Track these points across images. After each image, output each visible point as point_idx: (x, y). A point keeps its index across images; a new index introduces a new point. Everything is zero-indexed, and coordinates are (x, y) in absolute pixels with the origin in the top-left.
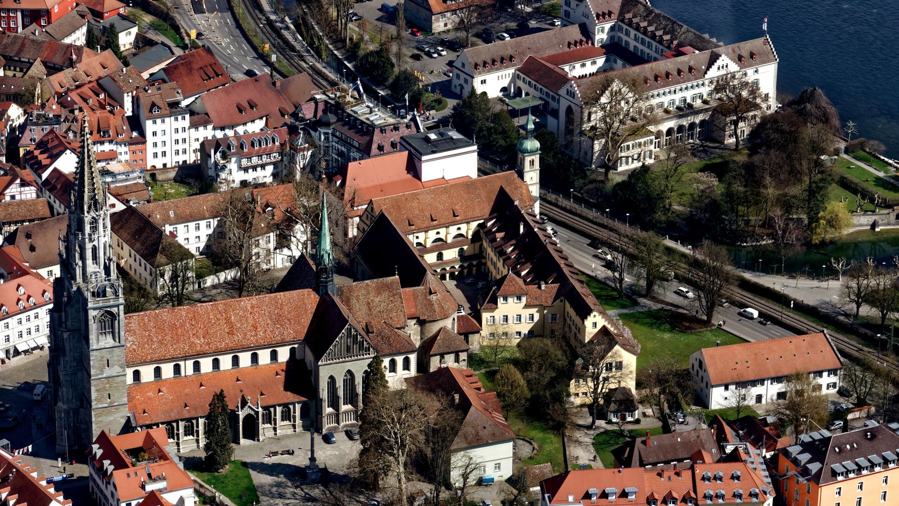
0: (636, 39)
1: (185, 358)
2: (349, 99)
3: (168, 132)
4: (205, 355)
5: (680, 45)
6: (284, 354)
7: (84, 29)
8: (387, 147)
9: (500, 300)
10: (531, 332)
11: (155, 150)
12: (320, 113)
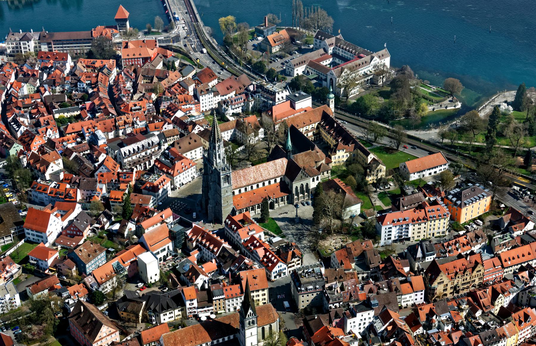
0: (342, 52)
1: (248, 186)
2: (264, 83)
4: (254, 184)
5: (359, 54)
6: (278, 180)
7: (162, 62)
8: (281, 99)
9: (337, 152)
10: (347, 160)
12: (255, 89)
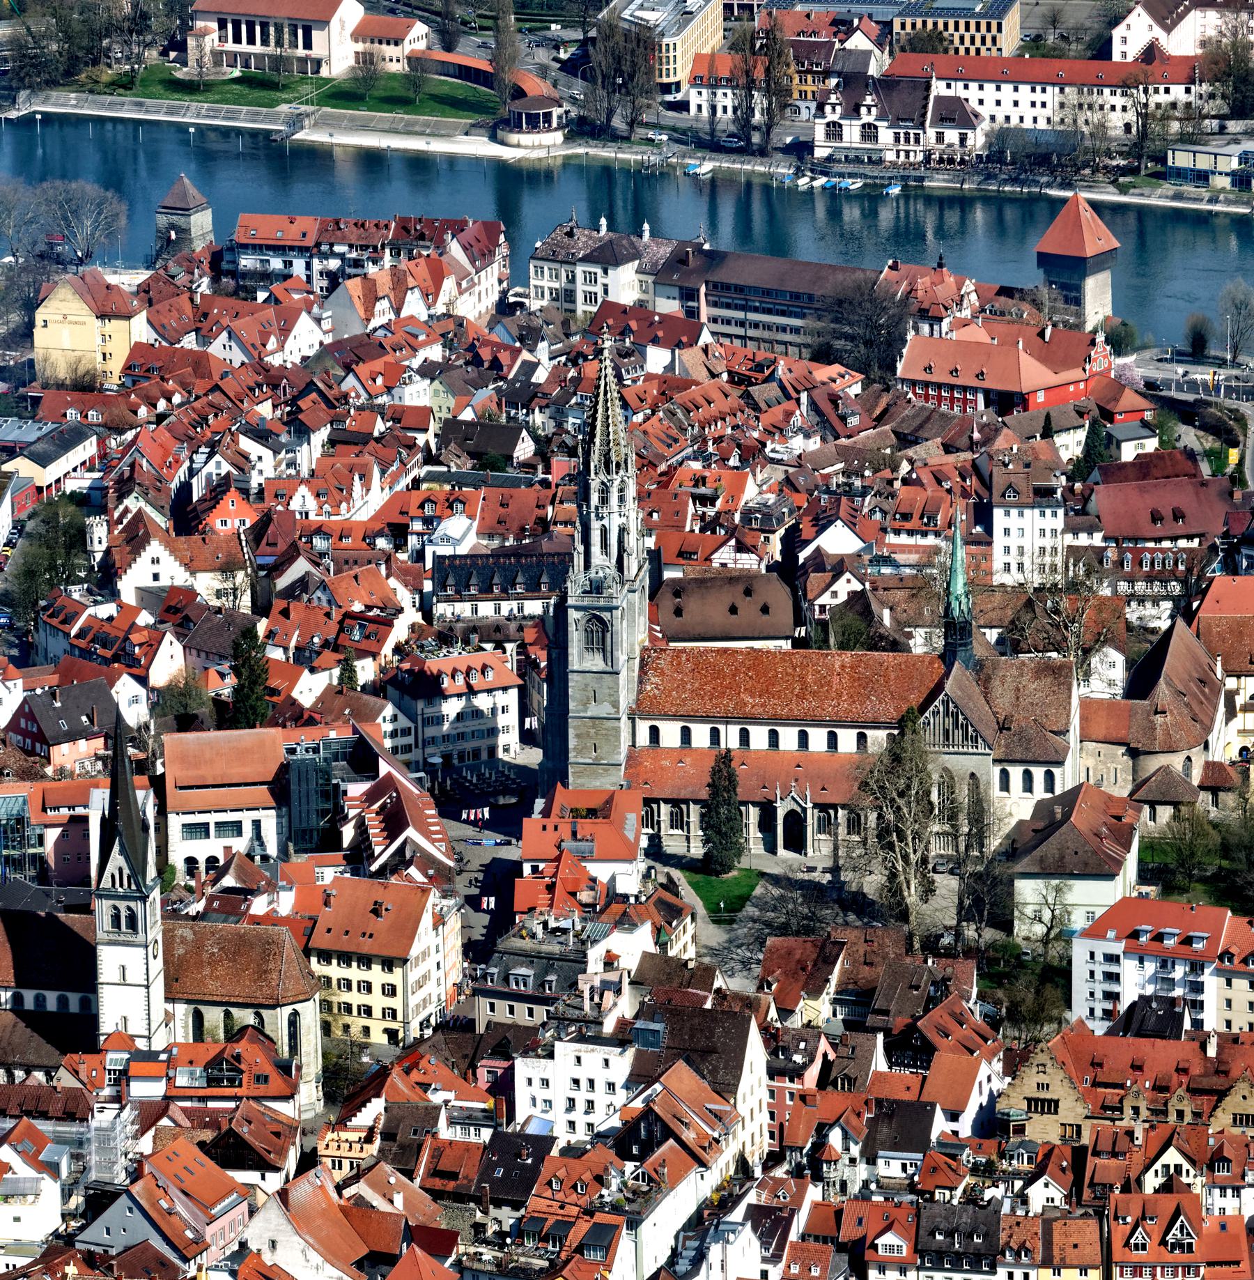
3: (1028, 532)
11: (1007, 559)
